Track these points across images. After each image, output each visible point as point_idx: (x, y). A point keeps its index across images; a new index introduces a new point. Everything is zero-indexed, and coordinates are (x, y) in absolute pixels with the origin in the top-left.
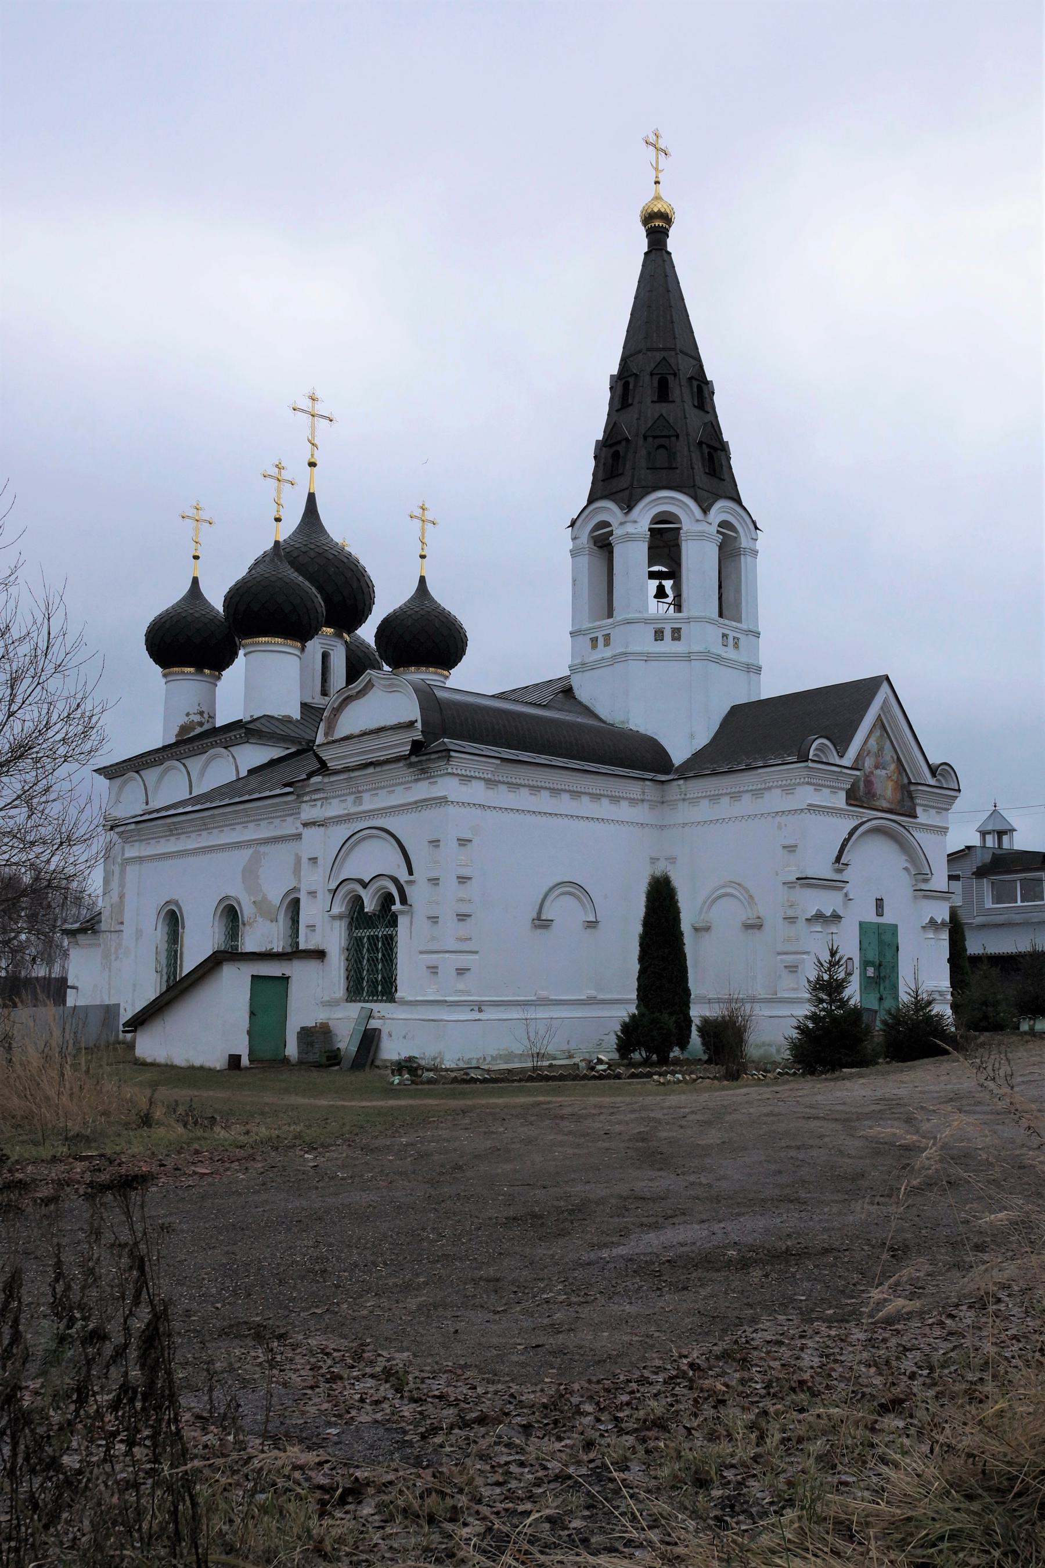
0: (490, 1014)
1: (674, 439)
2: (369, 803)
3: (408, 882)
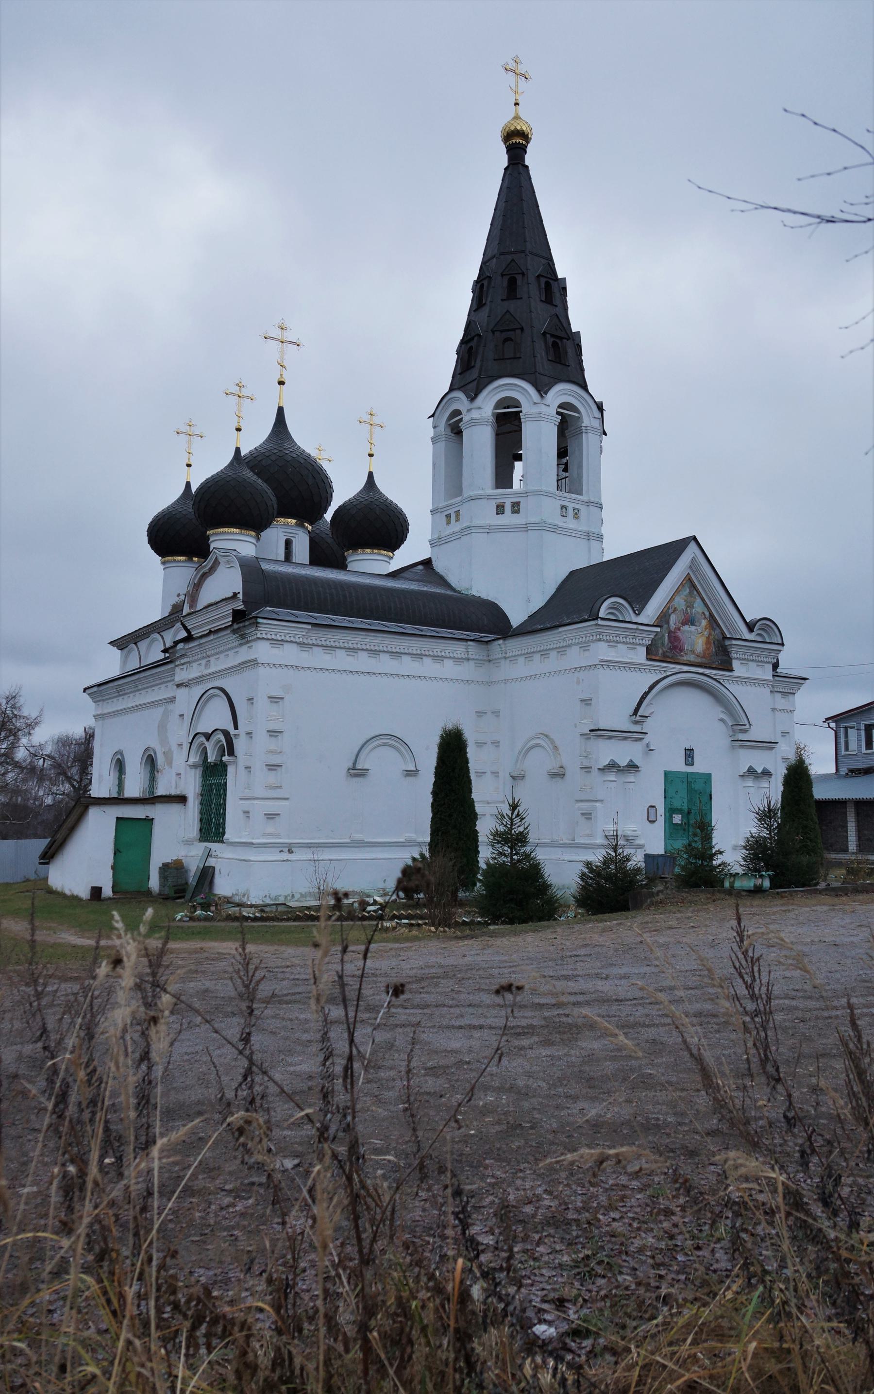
0: (300, 855)
1: (518, 332)
2: (216, 666)
3: (235, 735)
